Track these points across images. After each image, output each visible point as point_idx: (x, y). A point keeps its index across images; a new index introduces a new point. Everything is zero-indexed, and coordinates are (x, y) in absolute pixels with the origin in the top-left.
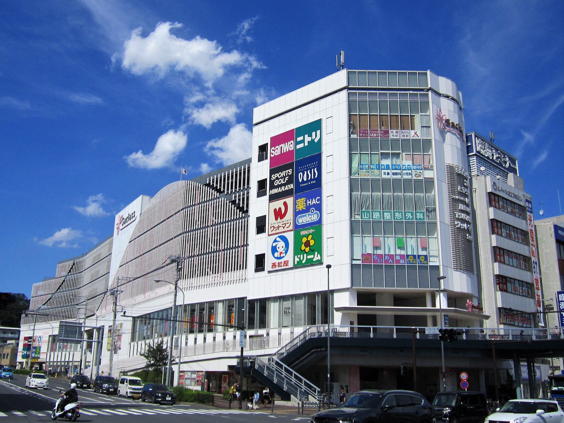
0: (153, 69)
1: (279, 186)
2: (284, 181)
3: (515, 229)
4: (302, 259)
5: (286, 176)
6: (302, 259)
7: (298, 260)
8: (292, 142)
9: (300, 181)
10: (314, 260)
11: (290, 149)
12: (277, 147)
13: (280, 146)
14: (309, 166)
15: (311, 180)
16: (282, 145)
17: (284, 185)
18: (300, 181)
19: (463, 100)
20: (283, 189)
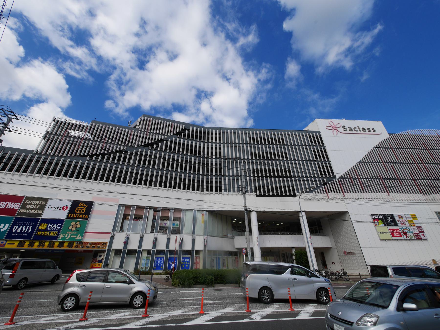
0: (134, 49)
1: (29, 209)
2: (36, 207)
3: (201, 281)
4: (66, 236)
5: (39, 205)
6: (66, 236)
7: (63, 237)
8: (19, 204)
9: (14, 231)
10: (76, 239)
11: (15, 208)
12: (4, 203)
13: (6, 203)
14: (26, 224)
15: (24, 233)
16: (8, 203)
17: (35, 210)
18: (14, 231)
19: (26, 325)
20: (33, 211)
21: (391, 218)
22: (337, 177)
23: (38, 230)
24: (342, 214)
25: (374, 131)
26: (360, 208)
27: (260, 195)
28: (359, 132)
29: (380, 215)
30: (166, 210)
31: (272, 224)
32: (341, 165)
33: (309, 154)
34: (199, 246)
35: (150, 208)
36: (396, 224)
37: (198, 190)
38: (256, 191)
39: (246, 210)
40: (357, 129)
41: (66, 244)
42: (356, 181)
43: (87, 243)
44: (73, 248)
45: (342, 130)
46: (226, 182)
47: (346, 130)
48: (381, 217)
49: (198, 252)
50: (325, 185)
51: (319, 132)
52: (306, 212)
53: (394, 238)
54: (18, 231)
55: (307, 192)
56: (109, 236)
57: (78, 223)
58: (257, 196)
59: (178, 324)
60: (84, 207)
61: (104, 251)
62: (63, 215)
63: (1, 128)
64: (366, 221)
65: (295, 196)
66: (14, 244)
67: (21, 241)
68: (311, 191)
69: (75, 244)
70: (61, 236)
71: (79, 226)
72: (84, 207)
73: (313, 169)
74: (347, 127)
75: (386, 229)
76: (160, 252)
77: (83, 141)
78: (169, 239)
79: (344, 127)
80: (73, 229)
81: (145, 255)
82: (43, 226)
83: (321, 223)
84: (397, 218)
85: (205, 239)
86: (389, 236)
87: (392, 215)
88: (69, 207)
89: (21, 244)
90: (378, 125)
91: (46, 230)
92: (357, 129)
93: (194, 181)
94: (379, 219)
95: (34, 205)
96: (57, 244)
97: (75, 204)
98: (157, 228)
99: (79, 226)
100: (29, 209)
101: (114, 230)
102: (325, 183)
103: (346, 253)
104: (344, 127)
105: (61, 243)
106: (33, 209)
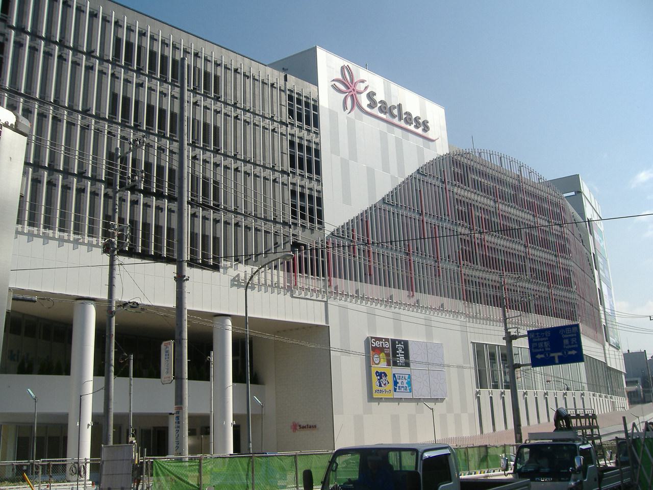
21: (403, 350)
25: (426, 128)
26: (352, 318)
28: (396, 121)
29: (387, 340)
31: (136, 343)
32: (345, 199)
33: (278, 202)
39: (183, 261)
40: (395, 112)
45: (364, 101)
47: (372, 105)
65: (216, 268)
77: (520, 317)
79: (371, 96)
83: (256, 352)
85: (320, 223)
92: (395, 112)
103: (296, 427)
104: (371, 96)
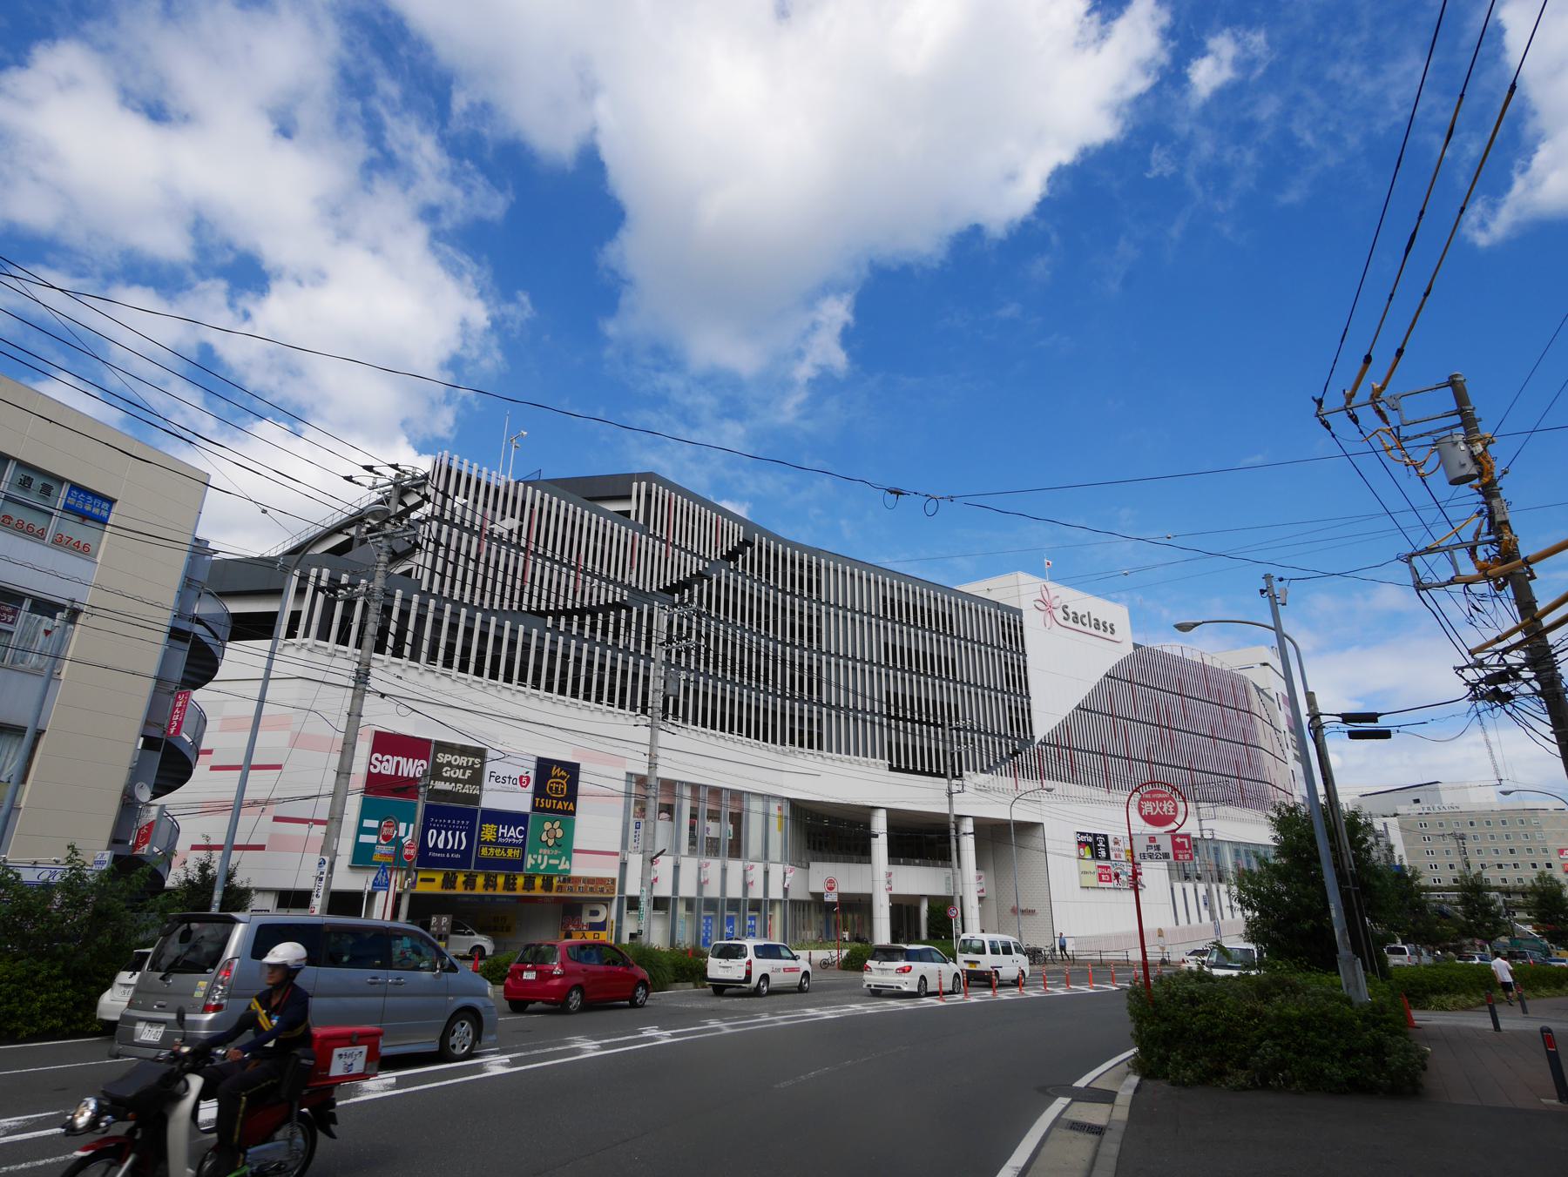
15: (444, 850)
22: (1037, 740)
23: (480, 842)
24: (1027, 829)
25: (1113, 632)
27: (898, 769)
28: (1087, 629)
30: (716, 792)
33: (990, 670)
34: (776, 893)
35: (687, 784)
36: (1108, 858)
37: (599, 700)
38: (890, 758)
40: (1086, 620)
41: (538, 882)
42: (1064, 758)
43: (577, 880)
44: (554, 894)
45: (1059, 615)
46: (831, 726)
48: (1090, 839)
49: (773, 902)
50: (569, 606)
51: (1019, 612)
52: (975, 818)
53: (1102, 884)
54: (441, 846)
55: (982, 771)
56: (617, 860)
57: (557, 824)
58: (891, 768)
59: (12, 1168)
60: (562, 778)
61: (606, 902)
62: (521, 801)
63: (1563, 953)
64: (131, 668)
66: (433, 880)
67: (446, 875)
68: (990, 770)
69: (555, 881)
70: (530, 861)
71: (559, 833)
72: (562, 778)
73: (993, 715)
74: (1069, 611)
75: (1092, 865)
76: (711, 904)
78: (724, 870)
80: (551, 842)
81: (681, 909)
82: (489, 831)
84: (1111, 844)
86: (1093, 880)
87: (1106, 836)
88: (532, 775)
89: (449, 882)
90: (1115, 612)
91: (496, 844)
93: (553, 653)
94: (1087, 843)
95: (459, 767)
96: (520, 881)
97: (545, 767)
98: (702, 845)
99: (559, 833)
100: (449, 780)
101: (624, 845)
102: (1016, 753)
105: (529, 881)
106: (457, 781)
